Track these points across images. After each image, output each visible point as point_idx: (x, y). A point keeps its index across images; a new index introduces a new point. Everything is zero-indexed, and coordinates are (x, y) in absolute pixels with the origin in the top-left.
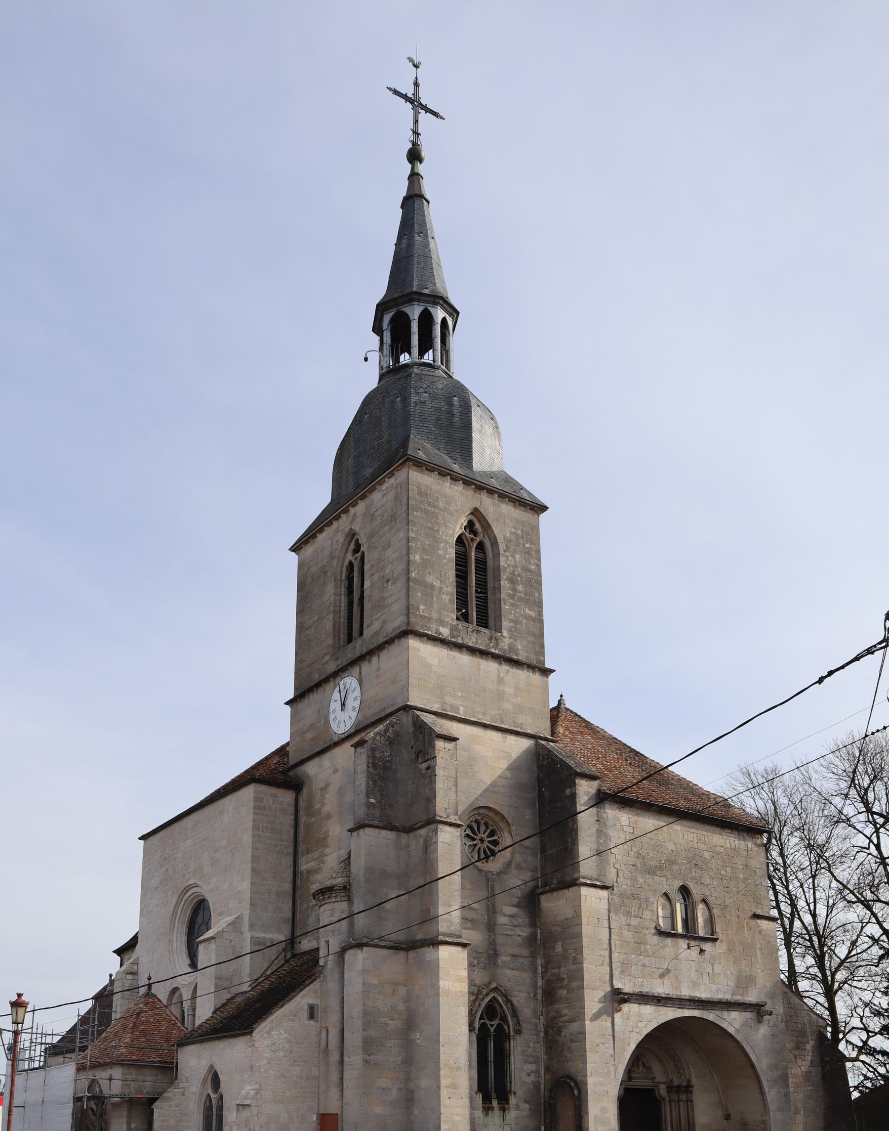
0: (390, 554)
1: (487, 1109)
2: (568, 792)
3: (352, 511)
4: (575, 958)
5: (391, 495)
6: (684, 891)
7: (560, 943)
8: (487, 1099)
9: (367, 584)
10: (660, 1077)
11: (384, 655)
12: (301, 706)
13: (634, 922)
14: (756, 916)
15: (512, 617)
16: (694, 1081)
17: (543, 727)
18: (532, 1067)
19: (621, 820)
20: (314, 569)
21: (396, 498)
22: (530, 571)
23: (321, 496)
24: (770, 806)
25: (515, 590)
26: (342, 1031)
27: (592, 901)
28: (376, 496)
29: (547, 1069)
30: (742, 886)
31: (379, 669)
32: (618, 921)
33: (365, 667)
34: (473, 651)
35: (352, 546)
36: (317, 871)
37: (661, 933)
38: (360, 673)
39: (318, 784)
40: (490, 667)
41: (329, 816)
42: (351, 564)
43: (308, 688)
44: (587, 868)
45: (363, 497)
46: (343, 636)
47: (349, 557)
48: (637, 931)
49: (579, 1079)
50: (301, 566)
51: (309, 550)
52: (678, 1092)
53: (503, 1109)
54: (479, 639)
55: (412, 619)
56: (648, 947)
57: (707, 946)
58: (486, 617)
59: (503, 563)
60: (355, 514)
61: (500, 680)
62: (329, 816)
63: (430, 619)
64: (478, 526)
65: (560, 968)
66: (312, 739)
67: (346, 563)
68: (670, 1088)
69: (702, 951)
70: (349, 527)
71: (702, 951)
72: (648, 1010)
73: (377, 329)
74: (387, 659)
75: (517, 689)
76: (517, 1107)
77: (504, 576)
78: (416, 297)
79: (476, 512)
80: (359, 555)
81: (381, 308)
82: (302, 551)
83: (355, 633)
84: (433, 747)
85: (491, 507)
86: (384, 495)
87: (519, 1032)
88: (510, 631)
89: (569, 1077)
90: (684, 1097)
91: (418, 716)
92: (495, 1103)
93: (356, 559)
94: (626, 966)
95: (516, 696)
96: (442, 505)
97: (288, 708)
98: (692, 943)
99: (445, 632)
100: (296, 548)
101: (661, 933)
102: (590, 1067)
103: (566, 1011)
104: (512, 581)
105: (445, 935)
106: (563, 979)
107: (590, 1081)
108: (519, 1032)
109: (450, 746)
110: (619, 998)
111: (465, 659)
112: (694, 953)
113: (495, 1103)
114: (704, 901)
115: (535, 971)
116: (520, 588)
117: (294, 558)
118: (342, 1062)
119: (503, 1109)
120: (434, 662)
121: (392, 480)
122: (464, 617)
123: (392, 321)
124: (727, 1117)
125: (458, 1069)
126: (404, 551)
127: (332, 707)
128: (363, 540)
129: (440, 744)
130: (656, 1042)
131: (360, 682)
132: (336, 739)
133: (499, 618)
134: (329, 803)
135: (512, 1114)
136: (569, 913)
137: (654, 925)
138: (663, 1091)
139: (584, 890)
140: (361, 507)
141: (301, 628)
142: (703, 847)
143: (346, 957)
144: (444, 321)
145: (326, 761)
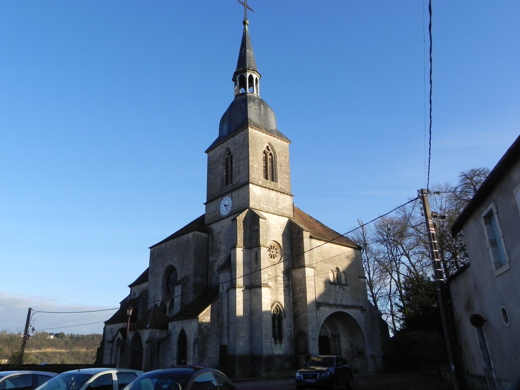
0: (353, 235)
1: (276, 343)
3: (228, 141)
5: (242, 137)
8: (275, 340)
9: (234, 166)
10: (329, 332)
11: (240, 190)
12: (209, 205)
14: (360, 277)
16: (341, 333)
17: (291, 213)
18: (289, 329)
20: (214, 159)
23: (215, 135)
24: (361, 237)
25: (281, 169)
26: (229, 316)
27: (309, 272)
28: (237, 137)
29: (294, 330)
33: (233, 194)
35: (228, 152)
36: (216, 261)
39: (216, 232)
42: (227, 159)
43: (212, 198)
44: (307, 262)
45: (232, 137)
46: (225, 183)
47: (227, 156)
51: (212, 153)
53: (281, 343)
54: (271, 184)
57: (345, 287)
58: (274, 179)
59: (278, 160)
61: (278, 199)
62: (220, 243)
64: (270, 148)
68: (332, 336)
69: (344, 290)
71: (344, 290)
72: (327, 309)
73: (234, 80)
74: (241, 191)
75: (282, 201)
76: (285, 343)
77: (278, 164)
80: (230, 156)
81: (236, 74)
83: (229, 182)
87: (285, 316)
90: (337, 339)
92: (278, 341)
96: (259, 140)
97: (205, 206)
99: (260, 183)
100: (207, 152)
103: (301, 310)
104: (280, 165)
108: (285, 316)
109: (264, 220)
112: (341, 290)
113: (278, 341)
115: (290, 296)
117: (206, 155)
118: (228, 327)
119: (281, 343)
121: (243, 132)
123: (240, 78)
128: (232, 151)
132: (223, 217)
135: (284, 345)
136: (302, 277)
138: (330, 336)
140: (231, 140)
144: (256, 78)
145: (219, 223)
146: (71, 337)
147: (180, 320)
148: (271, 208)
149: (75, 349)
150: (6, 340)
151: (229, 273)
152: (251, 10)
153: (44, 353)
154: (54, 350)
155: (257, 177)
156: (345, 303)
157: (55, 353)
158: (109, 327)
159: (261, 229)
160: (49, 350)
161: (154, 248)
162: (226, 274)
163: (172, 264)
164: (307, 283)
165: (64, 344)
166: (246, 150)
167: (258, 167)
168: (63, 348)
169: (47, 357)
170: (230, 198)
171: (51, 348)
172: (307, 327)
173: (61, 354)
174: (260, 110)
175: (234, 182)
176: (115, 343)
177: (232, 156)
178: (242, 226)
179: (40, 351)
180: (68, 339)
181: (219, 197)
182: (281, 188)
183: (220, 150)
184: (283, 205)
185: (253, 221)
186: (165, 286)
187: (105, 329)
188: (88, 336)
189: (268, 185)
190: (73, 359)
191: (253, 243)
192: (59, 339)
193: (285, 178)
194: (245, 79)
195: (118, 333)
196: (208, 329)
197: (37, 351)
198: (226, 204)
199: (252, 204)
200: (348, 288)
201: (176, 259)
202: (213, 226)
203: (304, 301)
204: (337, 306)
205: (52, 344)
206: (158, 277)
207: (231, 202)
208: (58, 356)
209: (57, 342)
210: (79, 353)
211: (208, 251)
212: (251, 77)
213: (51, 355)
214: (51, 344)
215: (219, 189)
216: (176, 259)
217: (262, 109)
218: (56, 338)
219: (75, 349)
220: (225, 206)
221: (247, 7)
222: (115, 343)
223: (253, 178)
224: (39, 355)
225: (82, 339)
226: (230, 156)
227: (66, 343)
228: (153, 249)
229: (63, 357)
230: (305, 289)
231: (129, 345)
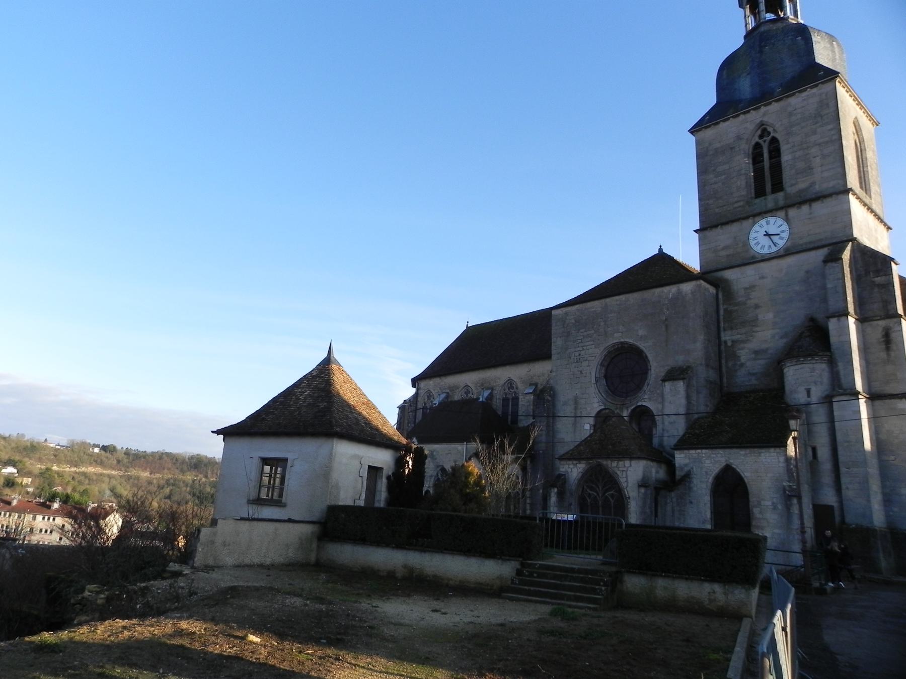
33: (792, 212)
35: (759, 132)
38: (787, 215)
50: (698, 143)
51: (709, 133)
62: (757, 307)
67: (753, 143)
127: (752, 235)
145: (750, 270)
146: (127, 453)
147: (772, 447)
149: (133, 472)
150: (25, 448)
151: (824, 366)
153: (84, 474)
154: (99, 470)
157: (101, 475)
160: (91, 470)
161: (565, 310)
162: (818, 366)
163: (631, 341)
165: (115, 462)
168: (113, 469)
169: (89, 480)
171: (94, 467)
173: (110, 477)
174: (833, 51)
178: (849, 276)
179: (78, 470)
180: (121, 456)
183: (741, 127)
188: (153, 454)
190: (128, 487)
192: (108, 454)
197: (73, 469)
199: (856, 234)
201: (641, 332)
205: (97, 461)
206: (585, 364)
208: (106, 479)
209: (104, 459)
210: (138, 478)
213: (94, 477)
214: (96, 461)
215: (741, 204)
217: (836, 50)
218: (103, 452)
219: (133, 472)
220: (767, 235)
224: (76, 476)
225: (144, 457)
226: (768, 139)
227: (119, 461)
229: (114, 482)
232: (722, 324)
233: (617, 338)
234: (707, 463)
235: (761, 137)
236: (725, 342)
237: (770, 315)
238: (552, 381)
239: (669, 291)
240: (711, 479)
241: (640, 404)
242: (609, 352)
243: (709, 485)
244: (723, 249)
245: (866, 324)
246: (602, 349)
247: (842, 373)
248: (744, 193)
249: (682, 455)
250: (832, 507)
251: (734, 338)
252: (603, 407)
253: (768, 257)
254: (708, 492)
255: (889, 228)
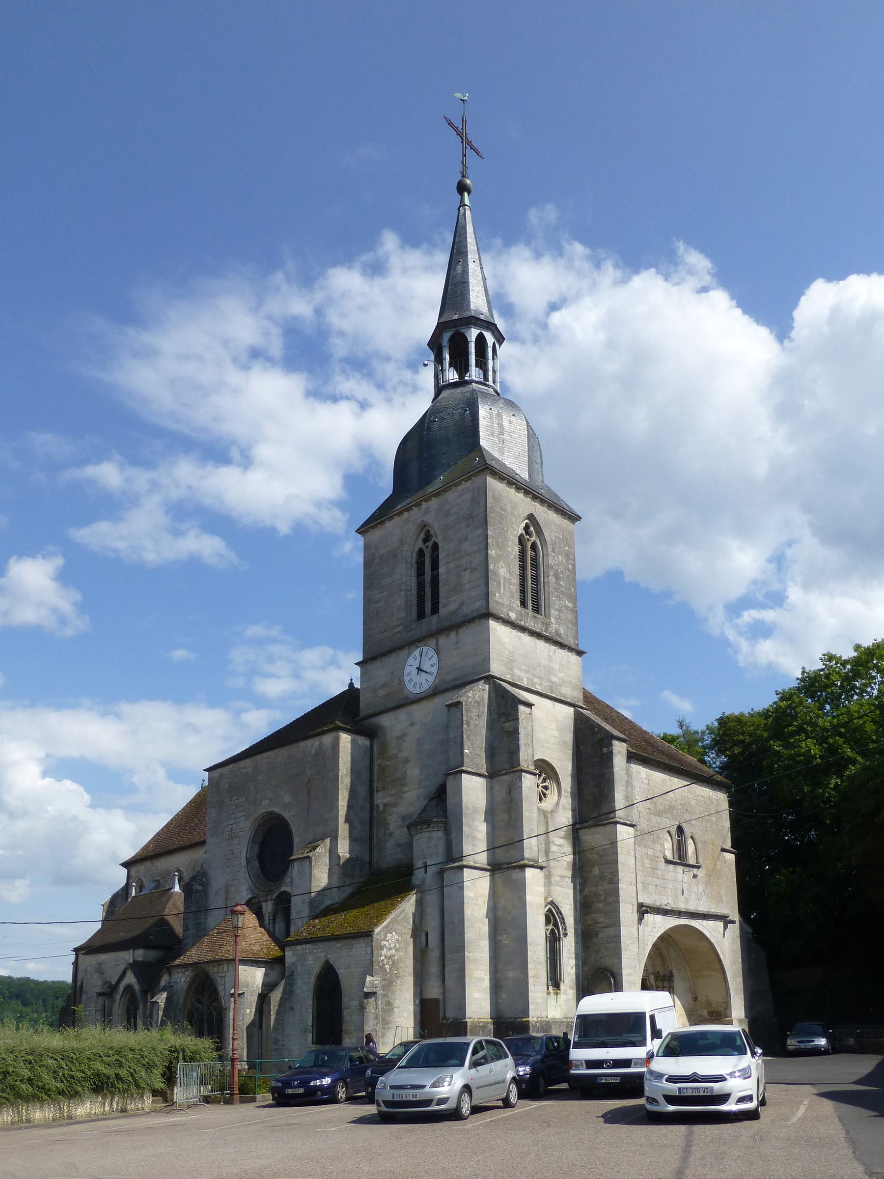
2: (605, 750)
4: (611, 879)
6: (680, 830)
7: (597, 867)
9: (442, 570)
13: (650, 852)
15: (556, 607)
16: (675, 973)
19: (641, 772)
20: (383, 551)
21: (473, 499)
22: (568, 569)
25: (559, 584)
30: (714, 827)
31: (457, 643)
32: (641, 851)
33: (443, 640)
34: (533, 633)
35: (422, 535)
36: (394, 805)
37: (668, 862)
38: (437, 644)
40: (541, 644)
41: (407, 761)
46: (414, 612)
47: (420, 544)
48: (653, 859)
49: (615, 971)
50: (367, 547)
51: (376, 534)
52: (663, 981)
55: (491, 604)
56: (659, 872)
60: (427, 508)
61: (550, 659)
62: (407, 761)
63: (503, 604)
65: (597, 886)
66: (385, 696)
67: (416, 549)
70: (421, 519)
72: (659, 918)
74: (466, 635)
75: (561, 665)
78: (474, 321)
79: (531, 517)
82: (368, 534)
84: (517, 710)
85: (544, 514)
86: (459, 496)
88: (556, 619)
89: (605, 969)
91: (500, 684)
93: (427, 547)
94: (645, 885)
95: (560, 671)
96: (509, 509)
98: (686, 869)
99: (513, 616)
101: (668, 862)
102: (624, 962)
104: (556, 576)
105: (528, 860)
106: (600, 895)
107: (624, 972)
108: (566, 935)
109: (527, 710)
110: (643, 910)
111: (526, 638)
114: (692, 837)
116: (562, 583)
120: (506, 640)
121: (469, 484)
122: (523, 604)
123: (451, 339)
124: (695, 999)
125: (540, 963)
126: (483, 546)
127: (407, 670)
129: (522, 708)
130: (666, 940)
131: (437, 651)
133: (548, 607)
134: (408, 749)
135: (562, 997)
137: (662, 855)
139: (619, 827)
141: (368, 602)
142: (692, 797)
143: (445, 876)
145: (402, 714)
148: (536, 680)
152: (478, 153)
155: (506, 601)
156: (692, 907)
158: (90, 961)
159: (521, 730)
161: (219, 771)
163: (277, 810)
164: (621, 858)
166: (480, 531)
167: (508, 576)
170: (431, 652)
172: (620, 958)
175: (443, 611)
176: (118, 997)
177: (435, 547)
181: (401, 647)
182: (557, 633)
183: (401, 530)
184: (561, 675)
185: (506, 707)
186: (256, 864)
187: (76, 964)
189: (530, 624)
191: (504, 761)
193: (566, 607)
194: (466, 342)
195: (124, 973)
196: (393, 963)
198: (420, 669)
200: (701, 873)
201: (287, 799)
202: (385, 721)
203: (610, 899)
204: (679, 914)
206: (236, 841)
207: (435, 660)
211: (371, 781)
212: (481, 339)
215: (400, 629)
216: (287, 799)
221: (469, 143)
222: (118, 997)
223: (498, 603)
226: (430, 544)
228: (216, 773)
230: (615, 873)
231: (181, 1001)
232: (375, 785)
233: (266, 807)
234: (311, 961)
235: (426, 540)
236: (378, 806)
237: (417, 772)
238: (205, 865)
239: (313, 745)
240: (313, 980)
241: (282, 890)
242: (260, 825)
243: (312, 987)
244: (381, 688)
245: (495, 780)
246: (252, 820)
247: (454, 841)
248: (403, 615)
249: (291, 953)
250: (438, 1000)
251: (387, 800)
252: (250, 896)
253: (419, 696)
254: (311, 996)
255: (580, 653)
